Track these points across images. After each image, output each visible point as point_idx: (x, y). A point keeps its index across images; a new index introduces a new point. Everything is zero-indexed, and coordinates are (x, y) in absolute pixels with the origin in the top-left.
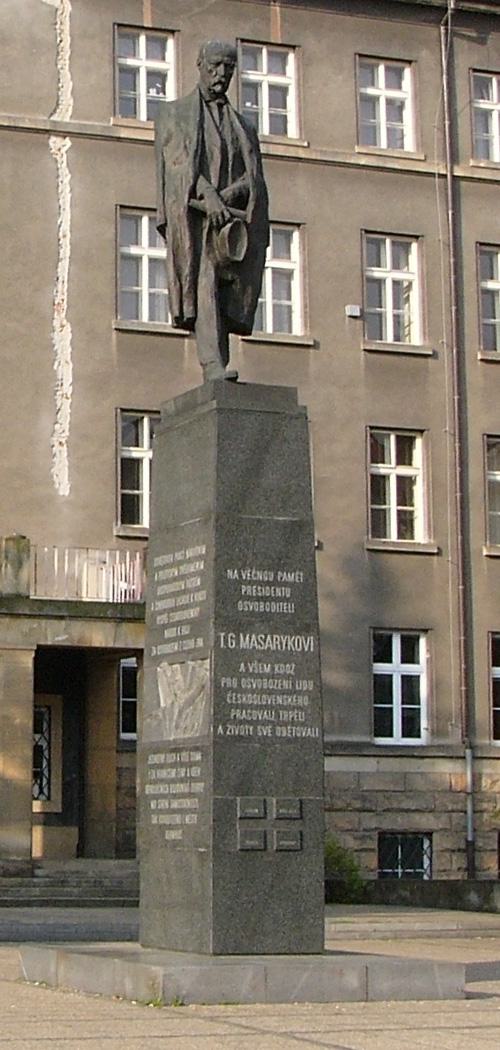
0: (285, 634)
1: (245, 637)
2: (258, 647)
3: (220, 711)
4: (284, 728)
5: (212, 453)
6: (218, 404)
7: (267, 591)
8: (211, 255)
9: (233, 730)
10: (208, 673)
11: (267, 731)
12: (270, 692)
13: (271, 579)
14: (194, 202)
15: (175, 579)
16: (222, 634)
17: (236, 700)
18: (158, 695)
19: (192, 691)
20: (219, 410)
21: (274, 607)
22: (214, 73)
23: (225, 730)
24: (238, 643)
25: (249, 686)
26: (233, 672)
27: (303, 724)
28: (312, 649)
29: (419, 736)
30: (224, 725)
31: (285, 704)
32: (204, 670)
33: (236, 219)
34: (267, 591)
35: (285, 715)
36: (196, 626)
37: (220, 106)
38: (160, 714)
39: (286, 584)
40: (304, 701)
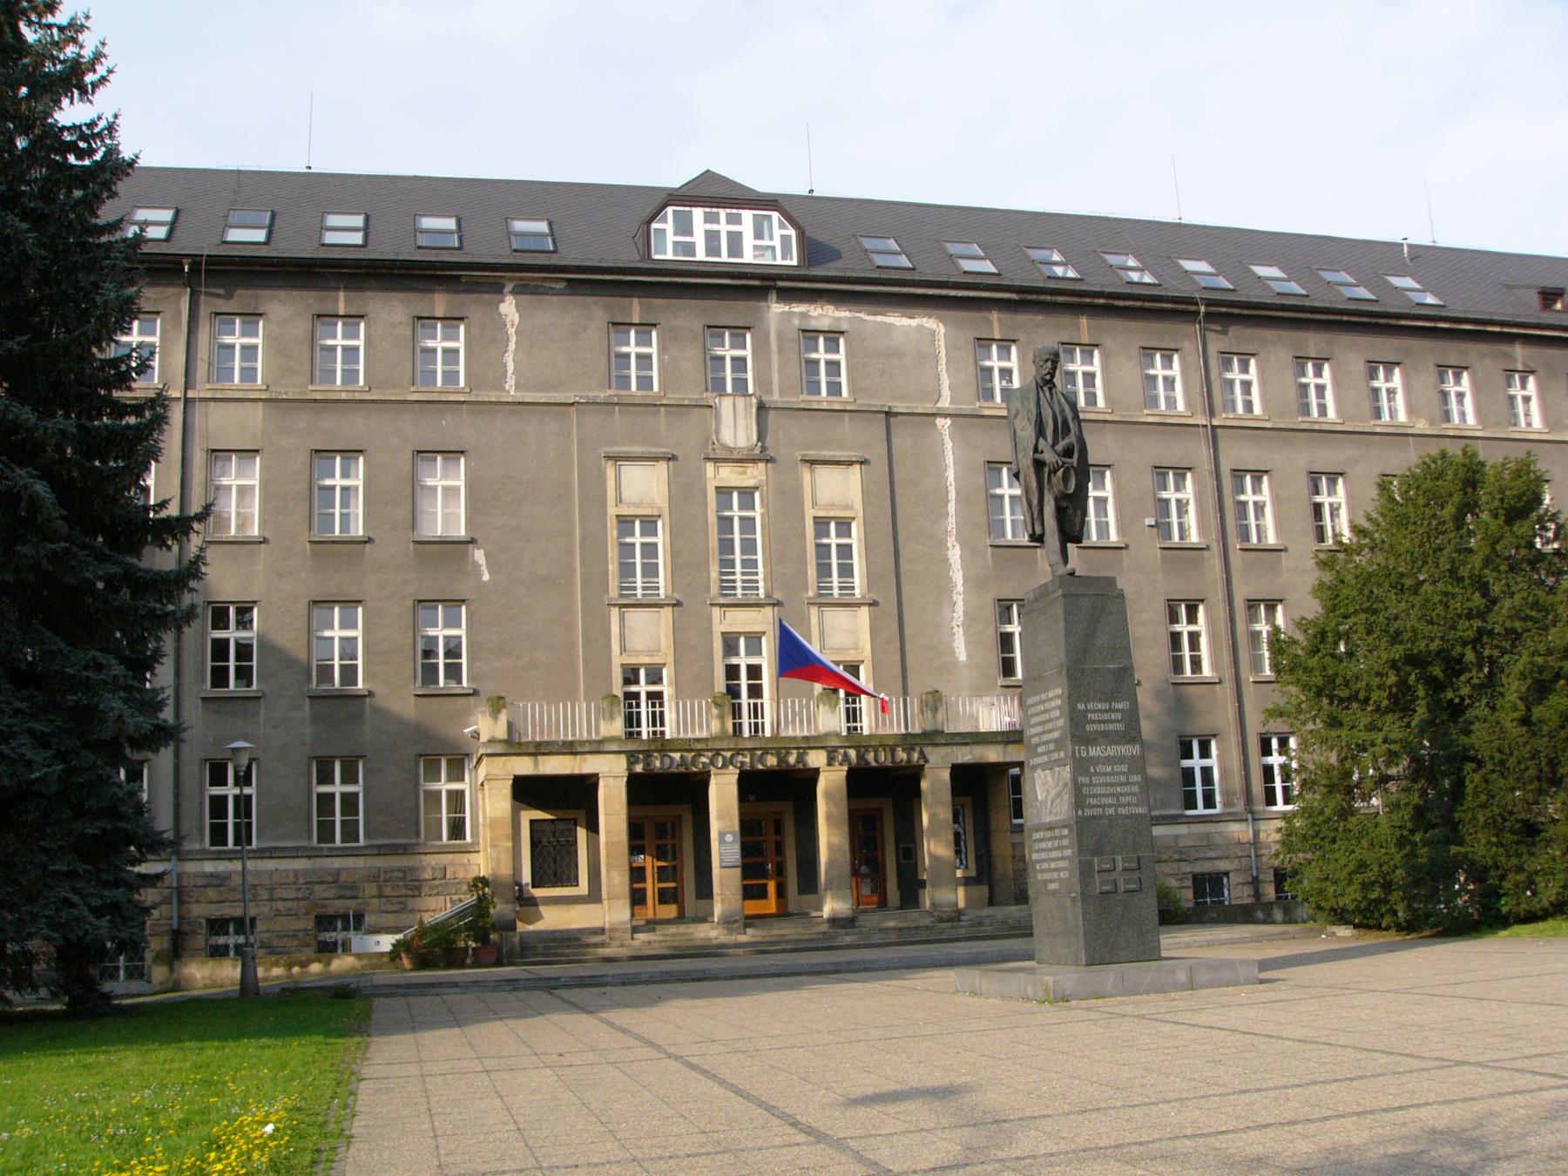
3: (1079, 800)
5: (1061, 625)
7: (1105, 716)
9: (1089, 812)
11: (1111, 811)
12: (1112, 785)
14: (1038, 456)
20: (1064, 596)
21: (1111, 727)
26: (1086, 773)
32: (1066, 773)
34: (1105, 716)
35: (1123, 800)
39: (1117, 711)
40: (1135, 789)
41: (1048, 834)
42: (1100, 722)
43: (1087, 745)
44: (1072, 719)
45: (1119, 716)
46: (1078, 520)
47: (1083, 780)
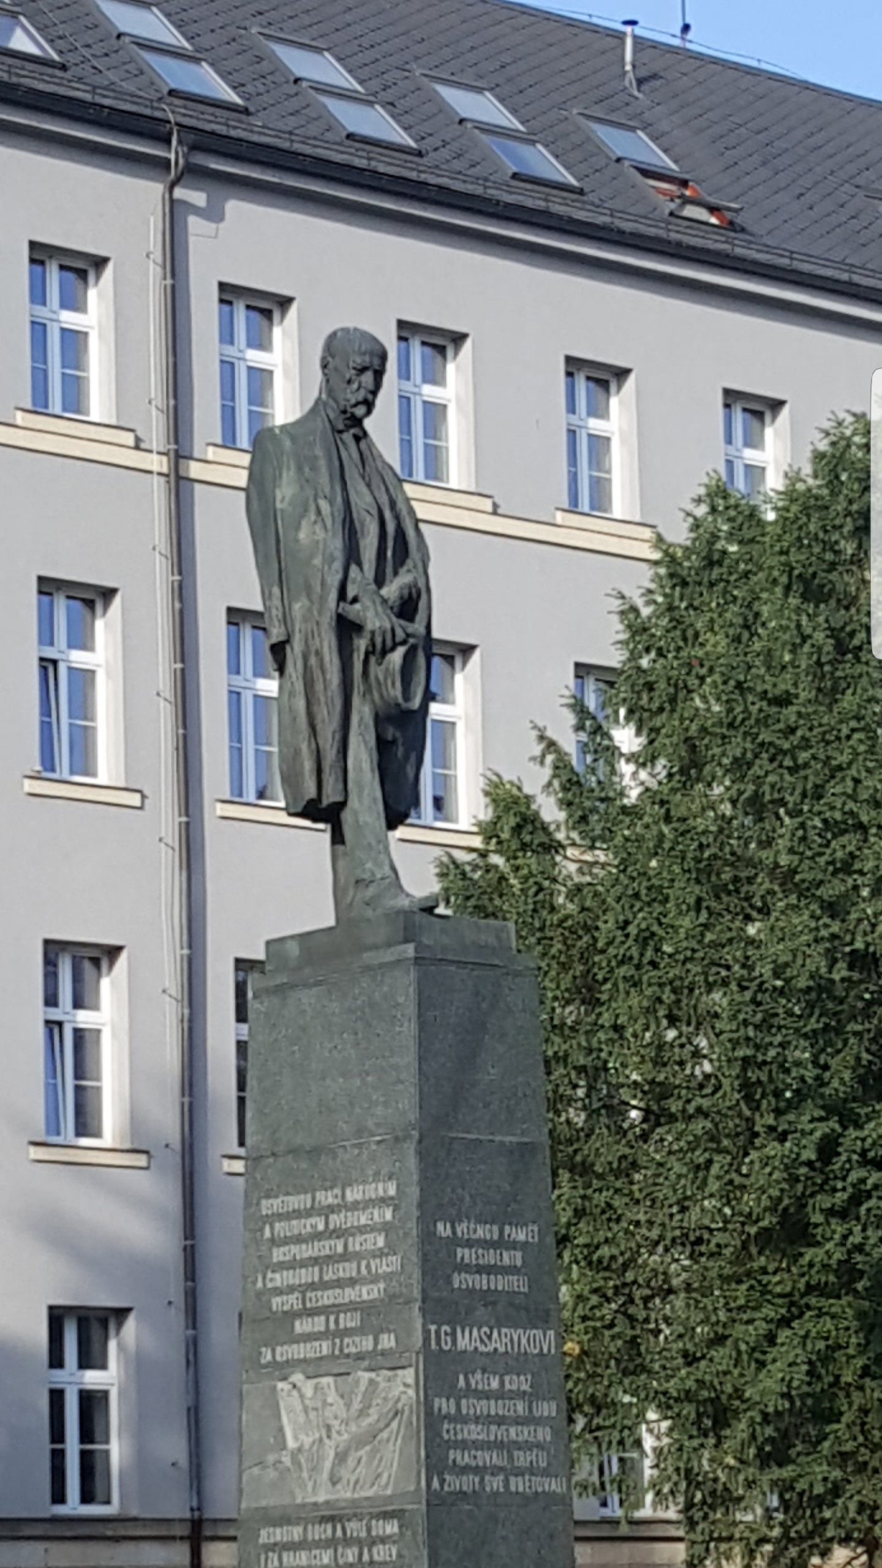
0: (516, 1327)
1: (463, 1332)
2: (482, 1348)
3: (436, 1455)
4: (520, 1479)
5: (408, 1030)
6: (416, 950)
7: (490, 1257)
8: (368, 697)
9: (453, 1483)
10: (411, 1392)
11: (495, 1483)
12: (500, 1421)
13: (496, 1237)
15: (317, 1236)
16: (433, 1328)
17: (455, 1434)
18: (281, 1430)
19: (370, 1420)
21: (500, 1283)
22: (355, 386)
23: (442, 1482)
24: (454, 1342)
25: (472, 1412)
26: (452, 1392)
27: (546, 1473)
28: (553, 1351)
29: (108, 1502)
30: (440, 1474)
31: (520, 1439)
32: (403, 1386)
33: (412, 641)
34: (490, 1257)
35: (522, 1459)
36: (373, 1316)
37: (357, 439)
38: (287, 1460)
39: (514, 1245)
40: (544, 1434)
41: (325, 1531)
42: (480, 1270)
43: (452, 1323)
44: (425, 1258)
45: (278, 1255)
46: (410, 771)
47: (444, 1405)
